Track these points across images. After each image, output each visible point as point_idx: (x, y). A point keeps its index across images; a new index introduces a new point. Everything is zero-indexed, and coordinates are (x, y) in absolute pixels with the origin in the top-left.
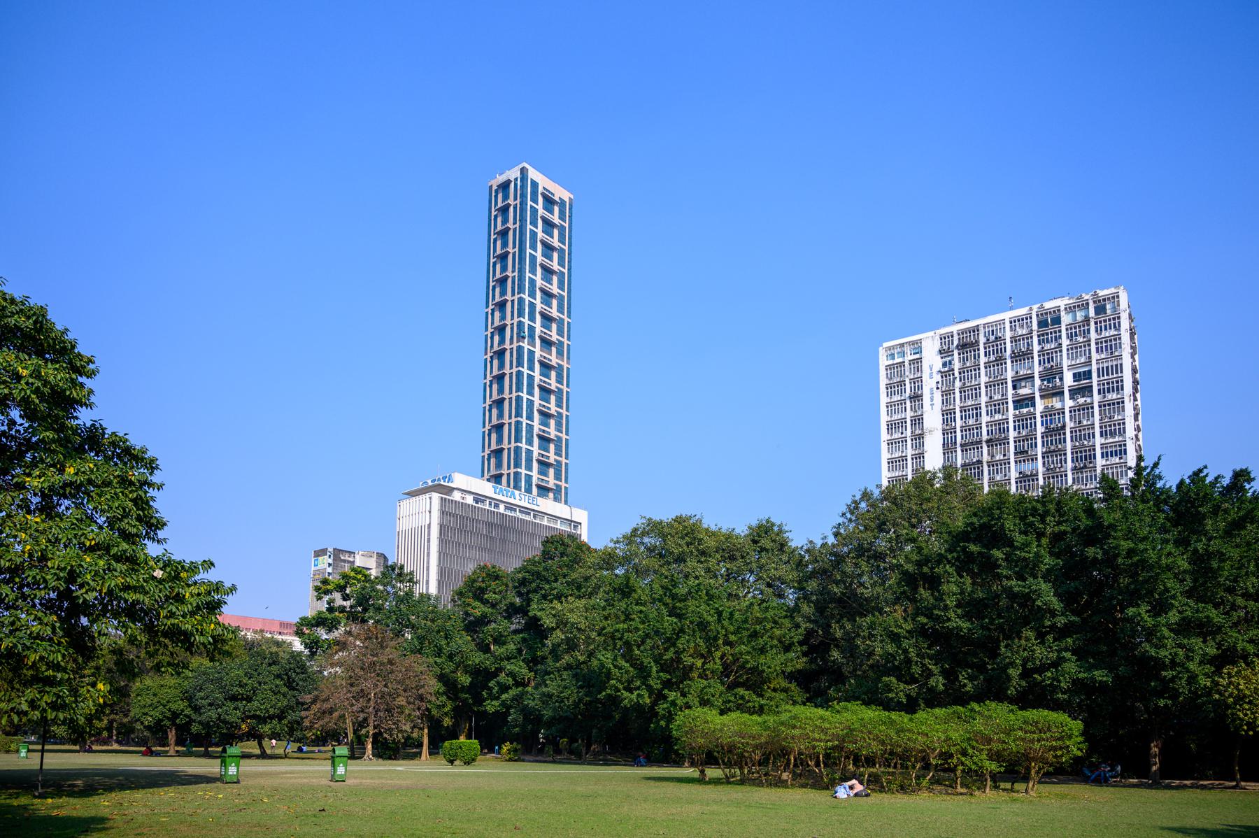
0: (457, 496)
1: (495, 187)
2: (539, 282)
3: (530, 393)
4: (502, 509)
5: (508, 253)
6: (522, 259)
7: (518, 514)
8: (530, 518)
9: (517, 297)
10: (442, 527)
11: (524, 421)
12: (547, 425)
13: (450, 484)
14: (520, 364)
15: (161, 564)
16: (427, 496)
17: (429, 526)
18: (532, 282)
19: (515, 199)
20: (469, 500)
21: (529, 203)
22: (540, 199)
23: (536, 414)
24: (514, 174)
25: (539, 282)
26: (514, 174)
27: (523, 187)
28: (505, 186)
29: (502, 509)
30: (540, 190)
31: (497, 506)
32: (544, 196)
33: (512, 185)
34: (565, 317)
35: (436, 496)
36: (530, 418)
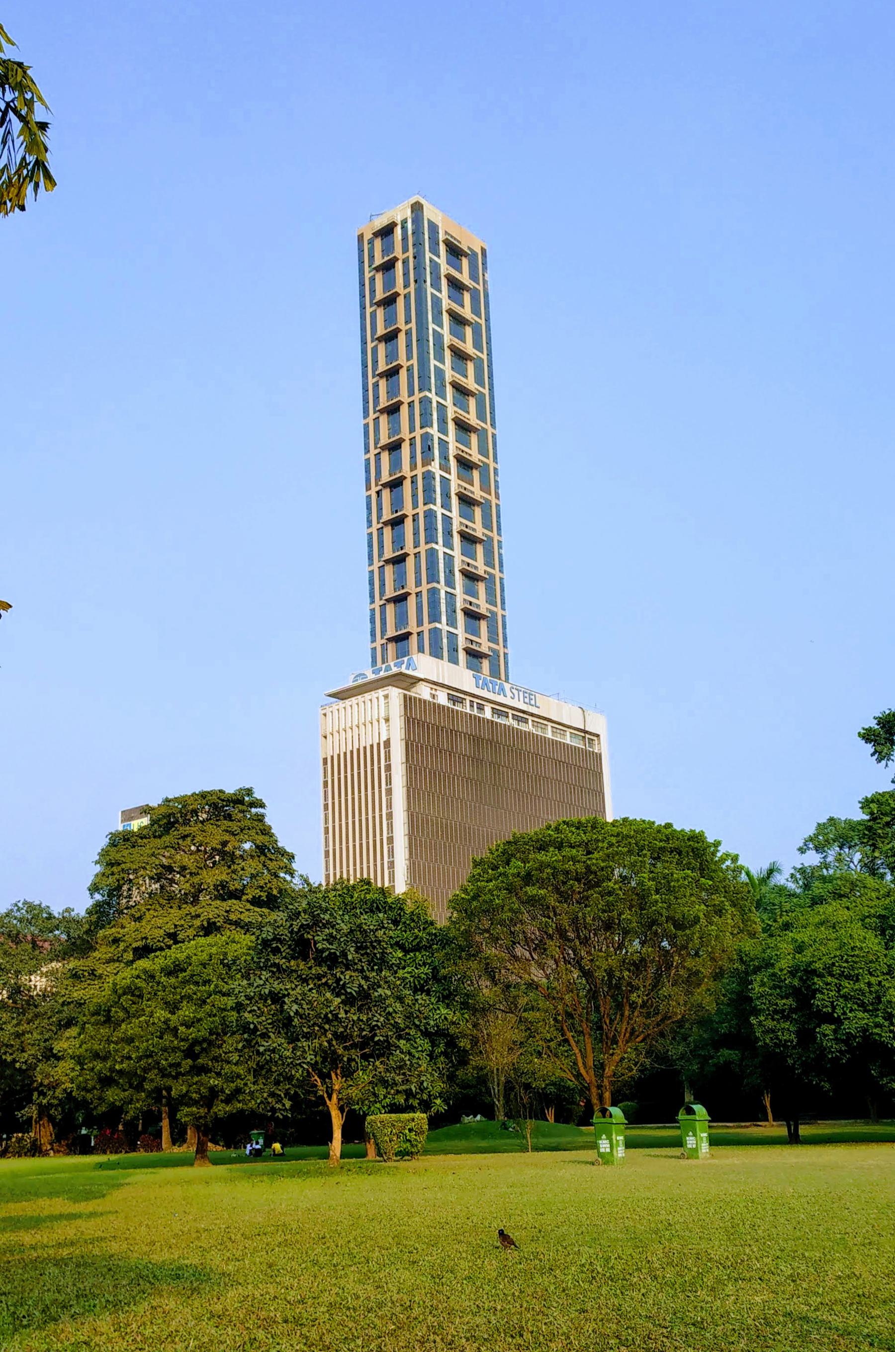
0: (423, 692)
1: (368, 236)
2: (449, 375)
3: (448, 544)
4: (488, 714)
5: (398, 330)
6: (422, 340)
7: (510, 722)
8: (529, 727)
9: (417, 396)
10: (410, 747)
11: (443, 589)
12: (475, 594)
13: (410, 672)
14: (430, 500)
15: (260, 839)
16: (381, 693)
17: (387, 743)
18: (440, 373)
19: (405, 249)
20: (442, 698)
21: (428, 255)
22: (442, 248)
23: (458, 576)
24: (401, 213)
25: (449, 375)
26: (401, 213)
27: (418, 232)
28: (386, 232)
29: (488, 714)
30: (442, 237)
31: (481, 708)
32: (447, 243)
33: (398, 231)
34: (488, 426)
35: (395, 694)
36: (450, 583)
